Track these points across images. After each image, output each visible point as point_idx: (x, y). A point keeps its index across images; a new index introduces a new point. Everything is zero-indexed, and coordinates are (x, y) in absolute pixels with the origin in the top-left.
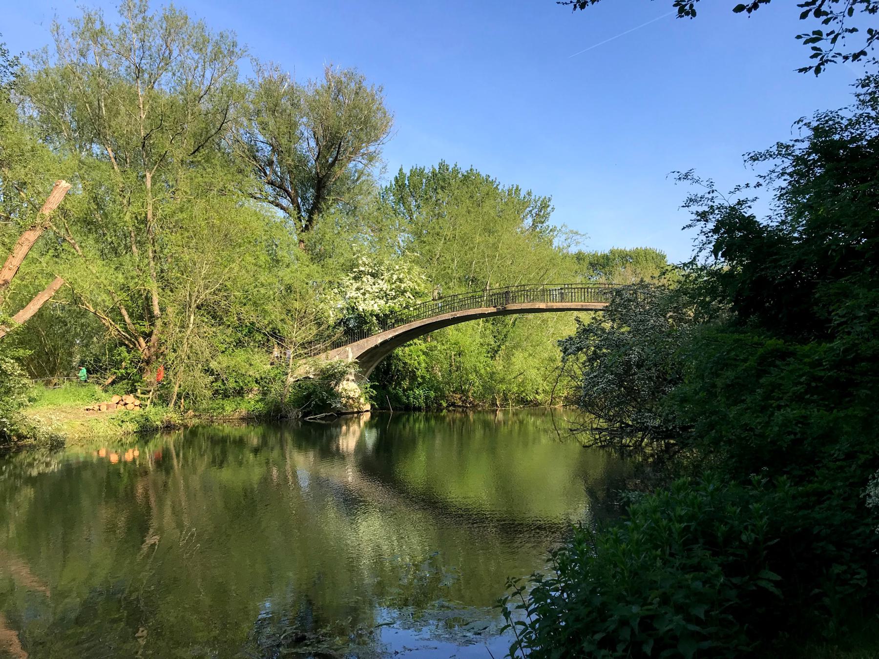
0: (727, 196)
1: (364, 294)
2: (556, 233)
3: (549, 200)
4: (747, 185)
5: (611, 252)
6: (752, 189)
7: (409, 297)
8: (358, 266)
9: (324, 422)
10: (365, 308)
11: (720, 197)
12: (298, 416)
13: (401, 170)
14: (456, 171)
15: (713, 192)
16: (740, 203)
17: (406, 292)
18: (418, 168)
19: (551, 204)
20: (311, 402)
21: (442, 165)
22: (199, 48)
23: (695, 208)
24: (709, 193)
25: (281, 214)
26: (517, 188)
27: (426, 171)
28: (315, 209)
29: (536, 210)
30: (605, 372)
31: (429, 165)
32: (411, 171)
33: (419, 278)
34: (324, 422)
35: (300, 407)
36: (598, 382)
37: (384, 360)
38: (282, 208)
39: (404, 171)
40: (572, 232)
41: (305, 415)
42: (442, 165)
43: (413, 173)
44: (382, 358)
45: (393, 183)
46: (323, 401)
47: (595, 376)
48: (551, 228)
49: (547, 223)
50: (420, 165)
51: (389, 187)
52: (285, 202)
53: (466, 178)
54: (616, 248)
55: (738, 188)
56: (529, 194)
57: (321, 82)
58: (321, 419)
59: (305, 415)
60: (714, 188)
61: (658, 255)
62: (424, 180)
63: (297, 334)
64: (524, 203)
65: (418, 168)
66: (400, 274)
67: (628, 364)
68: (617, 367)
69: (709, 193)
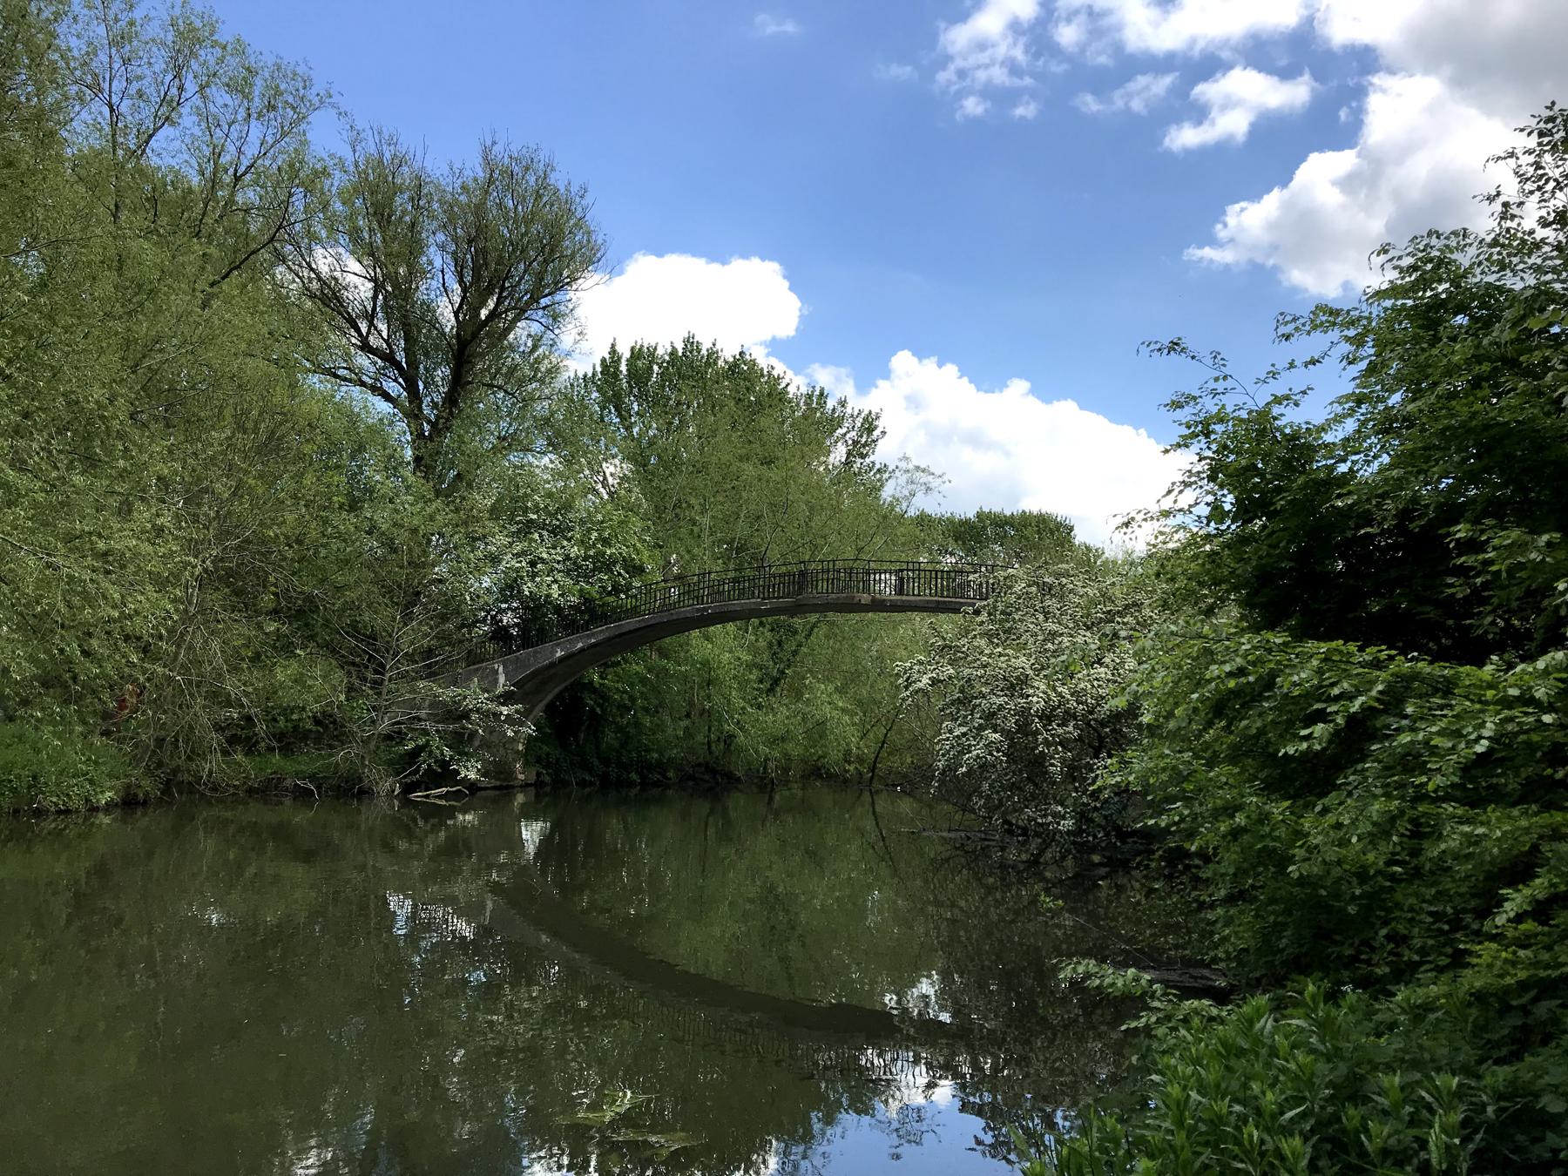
0: (1251, 389)
1: (533, 564)
2: (886, 475)
3: (877, 418)
4: (1292, 365)
5: (979, 515)
6: (1299, 371)
7: (620, 574)
8: (526, 510)
9: (444, 803)
10: (535, 590)
11: (1240, 389)
12: (393, 791)
13: (613, 346)
14: (713, 356)
15: (1225, 378)
16: (1278, 400)
17: (614, 563)
18: (646, 345)
19: (881, 424)
20: (419, 766)
21: (689, 342)
22: (240, 88)
23: (1186, 414)
24: (1216, 379)
25: (384, 407)
26: (822, 394)
27: (660, 351)
28: (729, 776)
29: (854, 433)
30: (981, 728)
31: (665, 338)
32: (633, 349)
33: (640, 540)
34: (444, 803)
35: (398, 774)
36: (970, 746)
37: (566, 689)
38: (386, 396)
39: (619, 349)
40: (917, 468)
41: (408, 788)
42: (689, 342)
43: (636, 354)
44: (563, 685)
45: (599, 369)
46: (444, 764)
47: (964, 734)
48: (877, 466)
49: (872, 458)
50: (648, 341)
51: (590, 375)
52: (393, 388)
53: (734, 367)
54: (986, 510)
55: (1274, 375)
56: (843, 403)
57: (475, 169)
58: (440, 797)
59: (408, 788)
60: (1226, 371)
61: (1059, 525)
62: (656, 368)
63: (412, 635)
64: (834, 422)
65: (646, 345)
66: (604, 529)
67: (1024, 712)
68: (1005, 717)
69: (1216, 379)
